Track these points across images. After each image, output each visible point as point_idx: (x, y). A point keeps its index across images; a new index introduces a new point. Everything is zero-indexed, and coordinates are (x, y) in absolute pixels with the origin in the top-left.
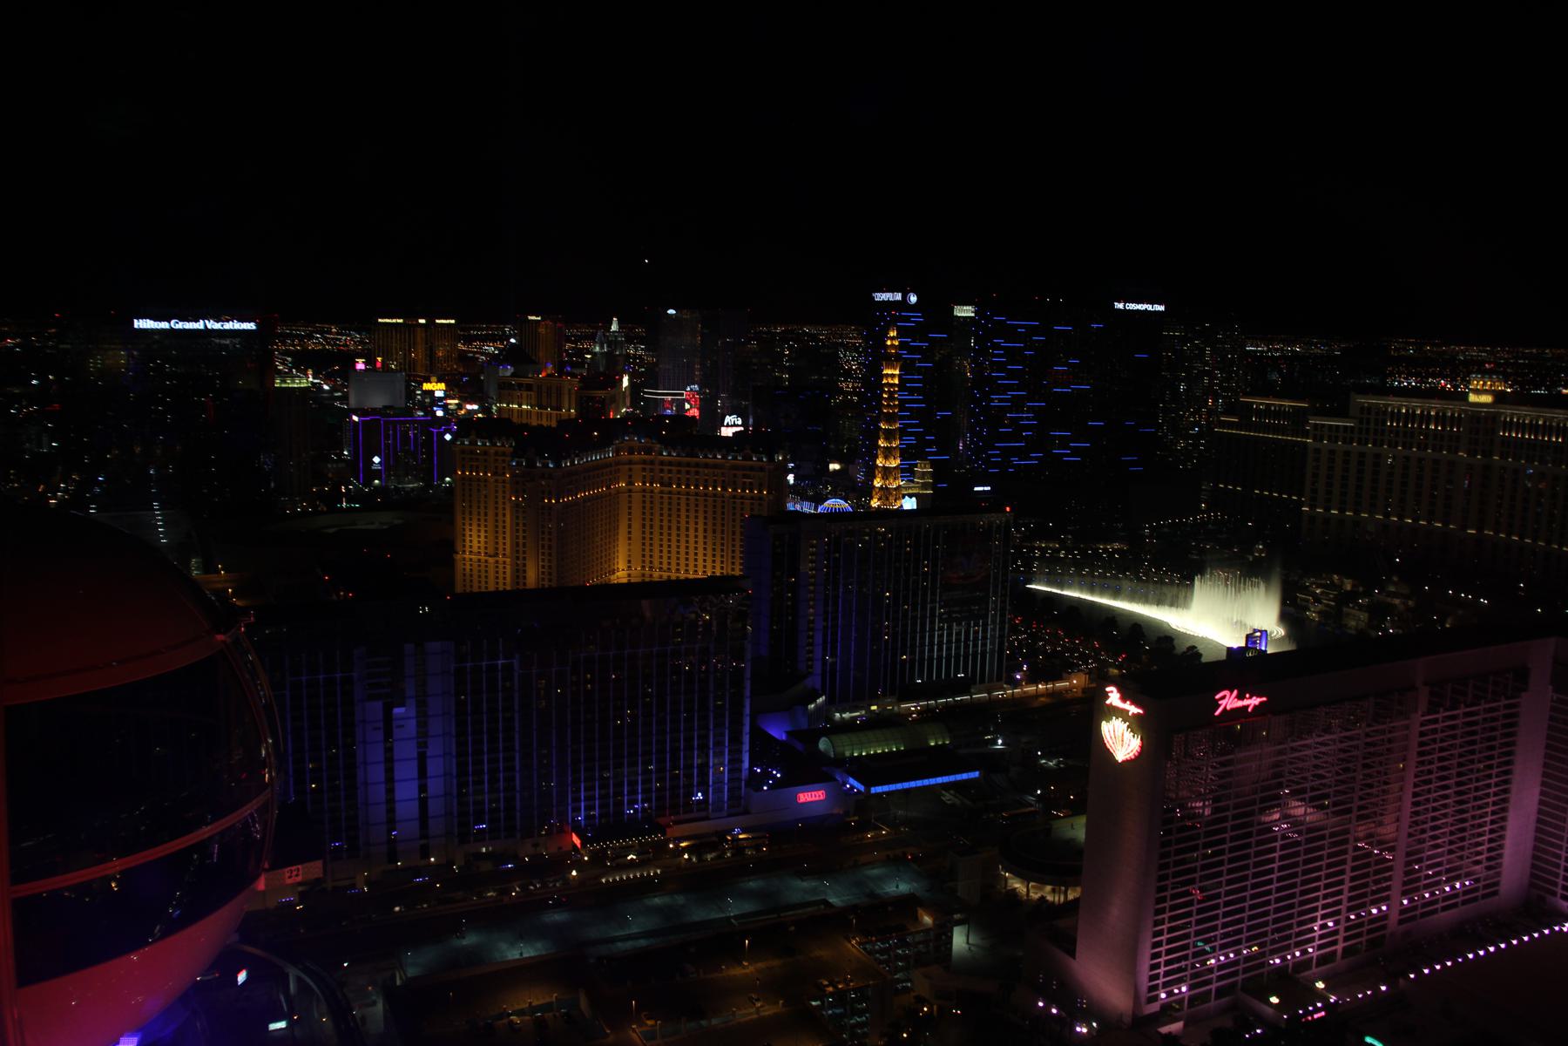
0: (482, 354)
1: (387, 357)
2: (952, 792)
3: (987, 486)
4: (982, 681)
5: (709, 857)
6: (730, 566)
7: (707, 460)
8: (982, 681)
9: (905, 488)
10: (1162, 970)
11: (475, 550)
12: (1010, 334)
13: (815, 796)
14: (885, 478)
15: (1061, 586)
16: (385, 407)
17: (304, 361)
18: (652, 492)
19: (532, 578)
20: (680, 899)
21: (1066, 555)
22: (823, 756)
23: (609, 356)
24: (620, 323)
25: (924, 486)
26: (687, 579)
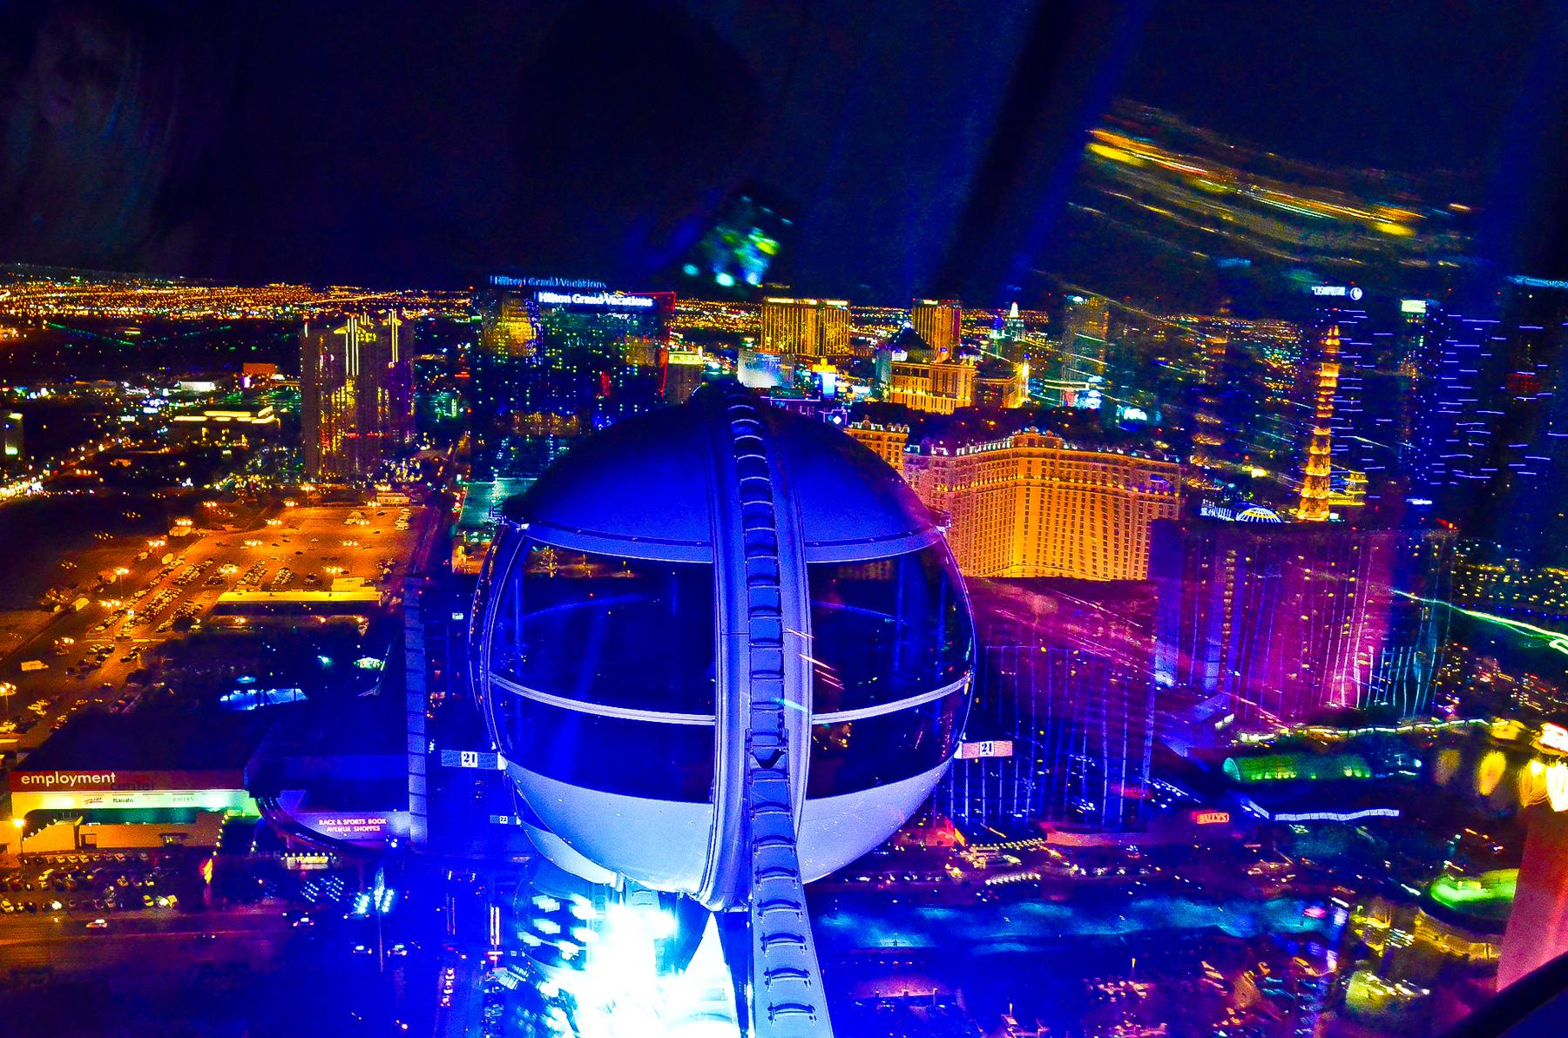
0: (874, 337)
2: (1364, 828)
3: (1427, 500)
4: (1409, 712)
5: (1100, 871)
6: (1133, 571)
7: (1143, 460)
9: (1333, 499)
11: (1050, 562)
12: (1465, 333)
13: (1216, 818)
14: (1314, 486)
16: (774, 388)
17: (694, 337)
18: (1051, 486)
20: (1067, 912)
21: (1512, 580)
22: (1227, 779)
23: (1007, 343)
24: (246, 436)
25: (1357, 498)
26: (1083, 581)
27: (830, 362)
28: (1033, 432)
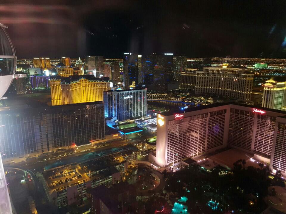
1: (37, 65)
8: (143, 116)
10: (169, 158)
15: (20, 170)
19: (66, 103)
24: (81, 58)
25: (134, 86)
26: (90, 102)
27: (47, 69)
28: (83, 79)
